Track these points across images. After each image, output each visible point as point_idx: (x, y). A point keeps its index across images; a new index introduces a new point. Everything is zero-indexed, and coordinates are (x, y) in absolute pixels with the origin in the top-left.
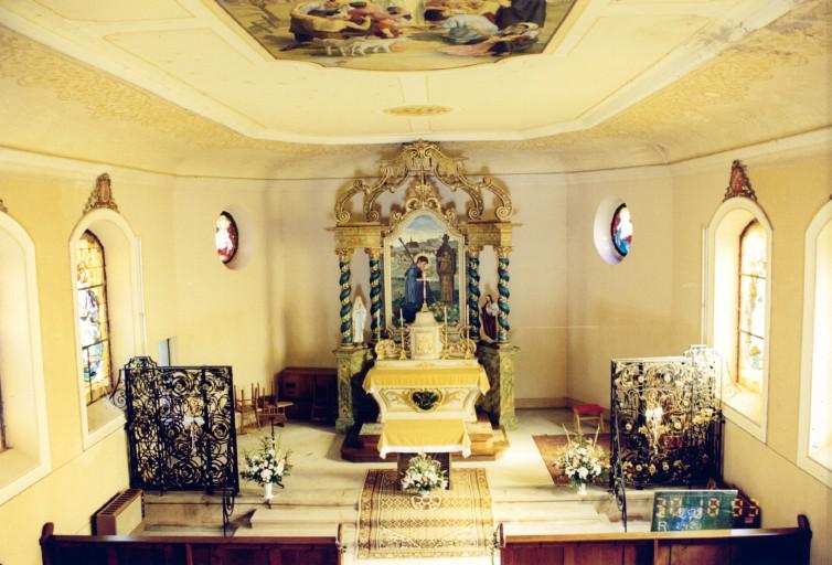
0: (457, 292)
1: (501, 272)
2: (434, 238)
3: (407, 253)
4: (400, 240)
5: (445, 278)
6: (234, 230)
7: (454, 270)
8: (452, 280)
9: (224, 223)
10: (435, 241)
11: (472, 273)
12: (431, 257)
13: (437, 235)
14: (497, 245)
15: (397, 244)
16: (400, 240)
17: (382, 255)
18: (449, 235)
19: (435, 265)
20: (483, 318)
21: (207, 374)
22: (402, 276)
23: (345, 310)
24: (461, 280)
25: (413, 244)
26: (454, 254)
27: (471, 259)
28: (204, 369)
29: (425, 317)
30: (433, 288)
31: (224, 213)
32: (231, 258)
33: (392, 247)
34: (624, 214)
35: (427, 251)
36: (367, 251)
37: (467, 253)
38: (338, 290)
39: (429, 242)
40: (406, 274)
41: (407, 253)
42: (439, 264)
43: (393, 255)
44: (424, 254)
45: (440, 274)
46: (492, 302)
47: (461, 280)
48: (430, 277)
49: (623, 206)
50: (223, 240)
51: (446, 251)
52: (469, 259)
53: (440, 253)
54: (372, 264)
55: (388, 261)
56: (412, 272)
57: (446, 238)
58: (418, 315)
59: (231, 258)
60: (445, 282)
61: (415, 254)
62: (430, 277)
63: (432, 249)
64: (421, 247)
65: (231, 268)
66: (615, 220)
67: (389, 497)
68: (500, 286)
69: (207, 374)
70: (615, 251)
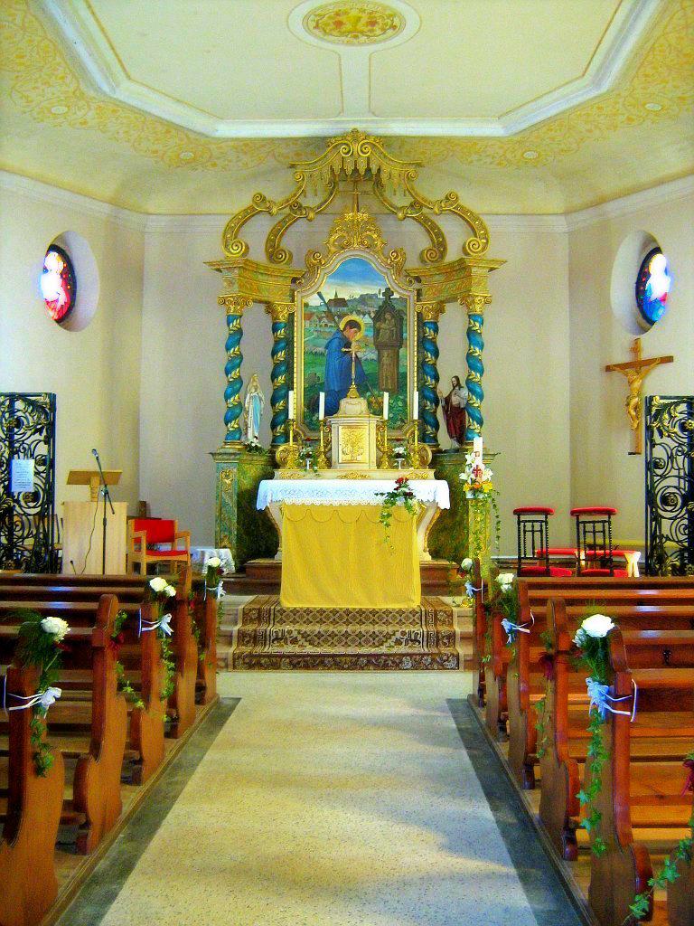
0: (404, 376)
1: (471, 333)
2: (371, 292)
3: (330, 315)
4: (319, 294)
5: (386, 354)
6: (69, 277)
7: (400, 342)
8: (396, 360)
9: (55, 262)
10: (371, 297)
11: (428, 345)
12: (365, 321)
13: (375, 290)
14: (466, 299)
15: (314, 301)
16: (319, 294)
17: (292, 315)
18: (393, 287)
19: (371, 334)
20: (445, 411)
21: (19, 405)
22: (321, 349)
23: (236, 386)
24: (410, 358)
25: (339, 302)
26: (400, 319)
27: (425, 324)
28: (13, 397)
29: (354, 405)
30: (368, 369)
31: (53, 248)
32: (65, 316)
33: (306, 305)
34: (657, 264)
35: (359, 313)
36: (270, 308)
37: (420, 315)
38: (223, 357)
39: (364, 299)
40: (326, 347)
41: (330, 315)
42: (377, 332)
43: (308, 317)
44: (354, 317)
45: (380, 347)
46: (460, 387)
47: (410, 358)
48: (363, 349)
49: (657, 250)
50: (53, 287)
51: (388, 311)
52: (421, 323)
53: (378, 317)
54: (275, 330)
55: (300, 328)
56: (336, 342)
57: (388, 293)
58: (343, 402)
59: (65, 316)
60: (385, 360)
61: (341, 317)
62: (363, 349)
63: (367, 309)
64: (350, 304)
65: (61, 326)
66: (643, 275)
67: (330, 131)
68: (469, 356)
69: (19, 405)
70: (640, 317)
